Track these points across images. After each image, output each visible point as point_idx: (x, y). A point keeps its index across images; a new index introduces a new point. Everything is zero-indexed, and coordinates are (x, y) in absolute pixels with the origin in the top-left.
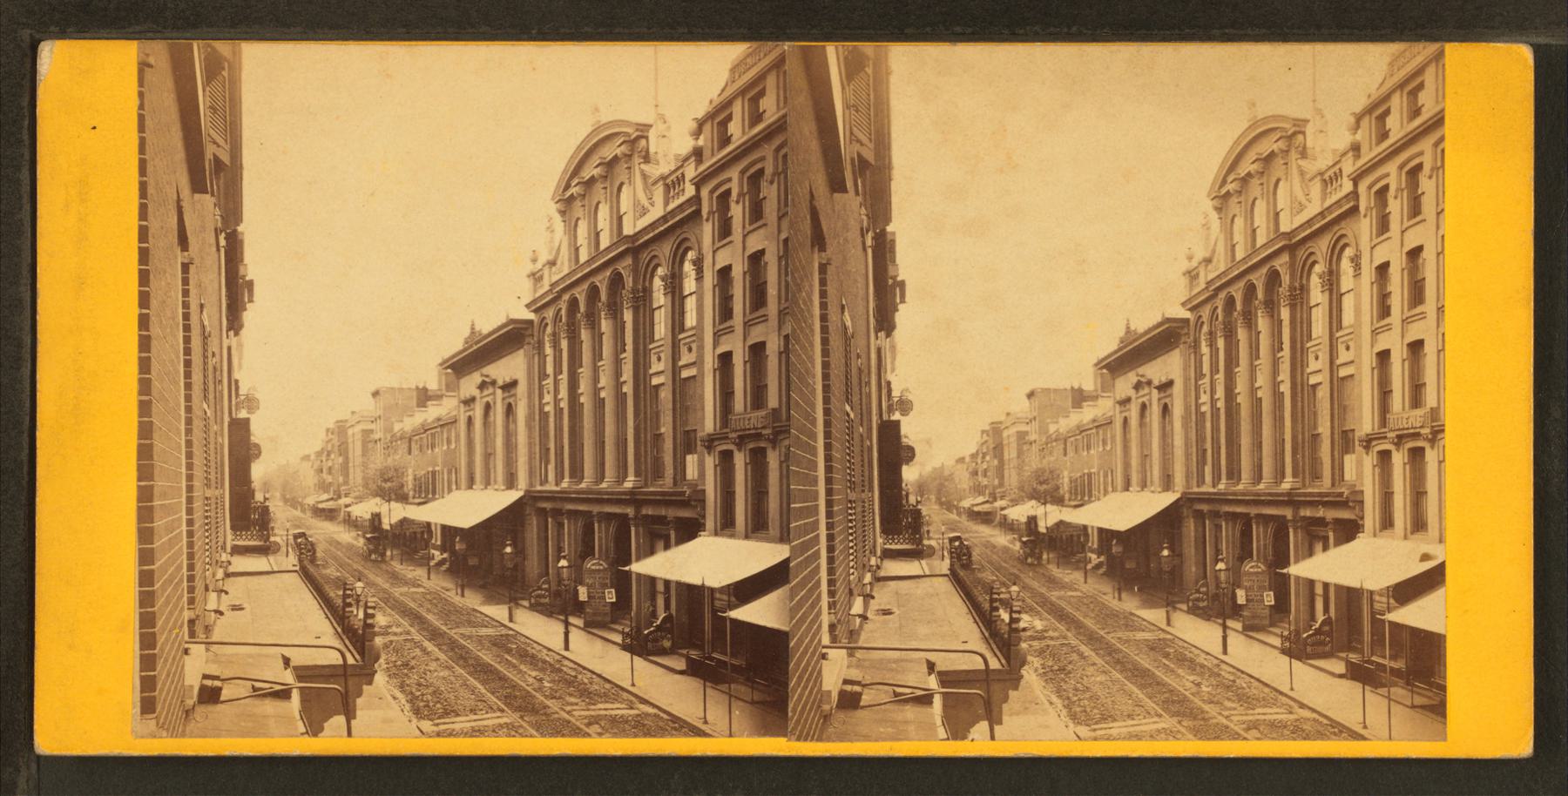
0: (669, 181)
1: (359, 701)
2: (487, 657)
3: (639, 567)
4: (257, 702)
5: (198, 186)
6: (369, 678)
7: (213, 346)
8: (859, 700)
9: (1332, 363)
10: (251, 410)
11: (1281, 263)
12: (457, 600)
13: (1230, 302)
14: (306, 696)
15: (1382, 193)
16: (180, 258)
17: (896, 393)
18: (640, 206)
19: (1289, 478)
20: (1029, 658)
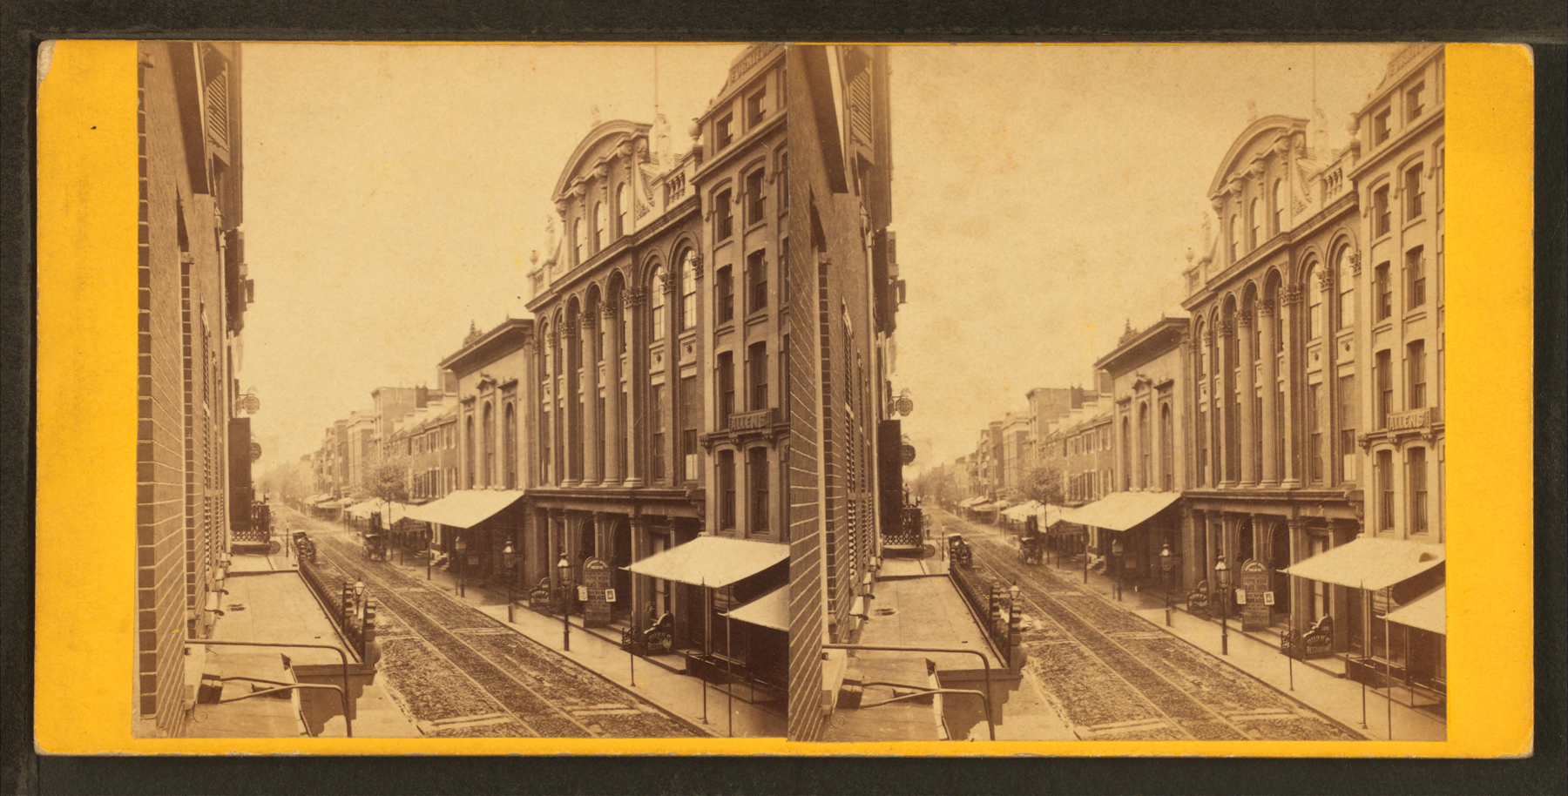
0: (669, 181)
1: (359, 701)
2: (487, 657)
3: (639, 567)
4: (257, 702)
5: (198, 186)
6: (369, 678)
7: (213, 346)
8: (859, 700)
9: (1332, 363)
10: (251, 410)
11: (624, 266)
12: (457, 599)
13: (1230, 302)
15: (1382, 193)
16: (180, 258)
17: (896, 393)
18: (640, 206)
19: (1289, 478)
20: (1029, 658)
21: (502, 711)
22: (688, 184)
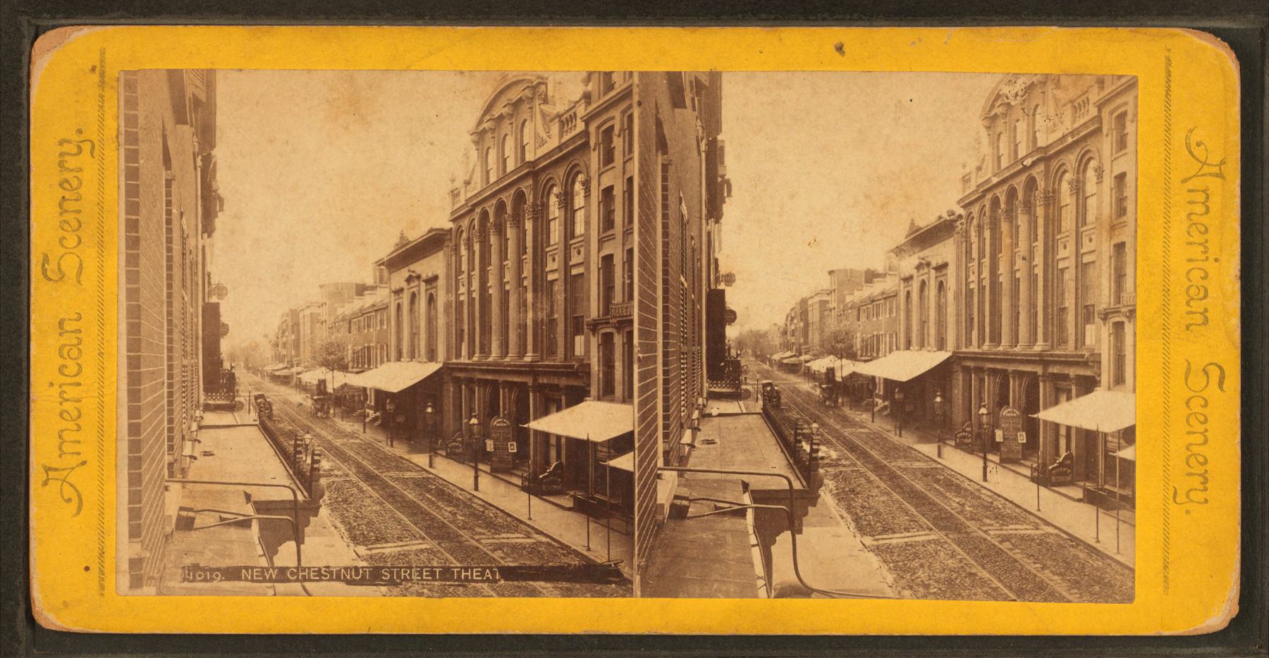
0: (563, 118)
1: (307, 530)
2: (411, 496)
3: (534, 425)
5: (180, 119)
9: (1077, 251)
10: (220, 296)
12: (387, 449)
14: (264, 526)
16: (164, 174)
18: (540, 139)
19: (1040, 342)
20: (826, 481)
21: (423, 539)
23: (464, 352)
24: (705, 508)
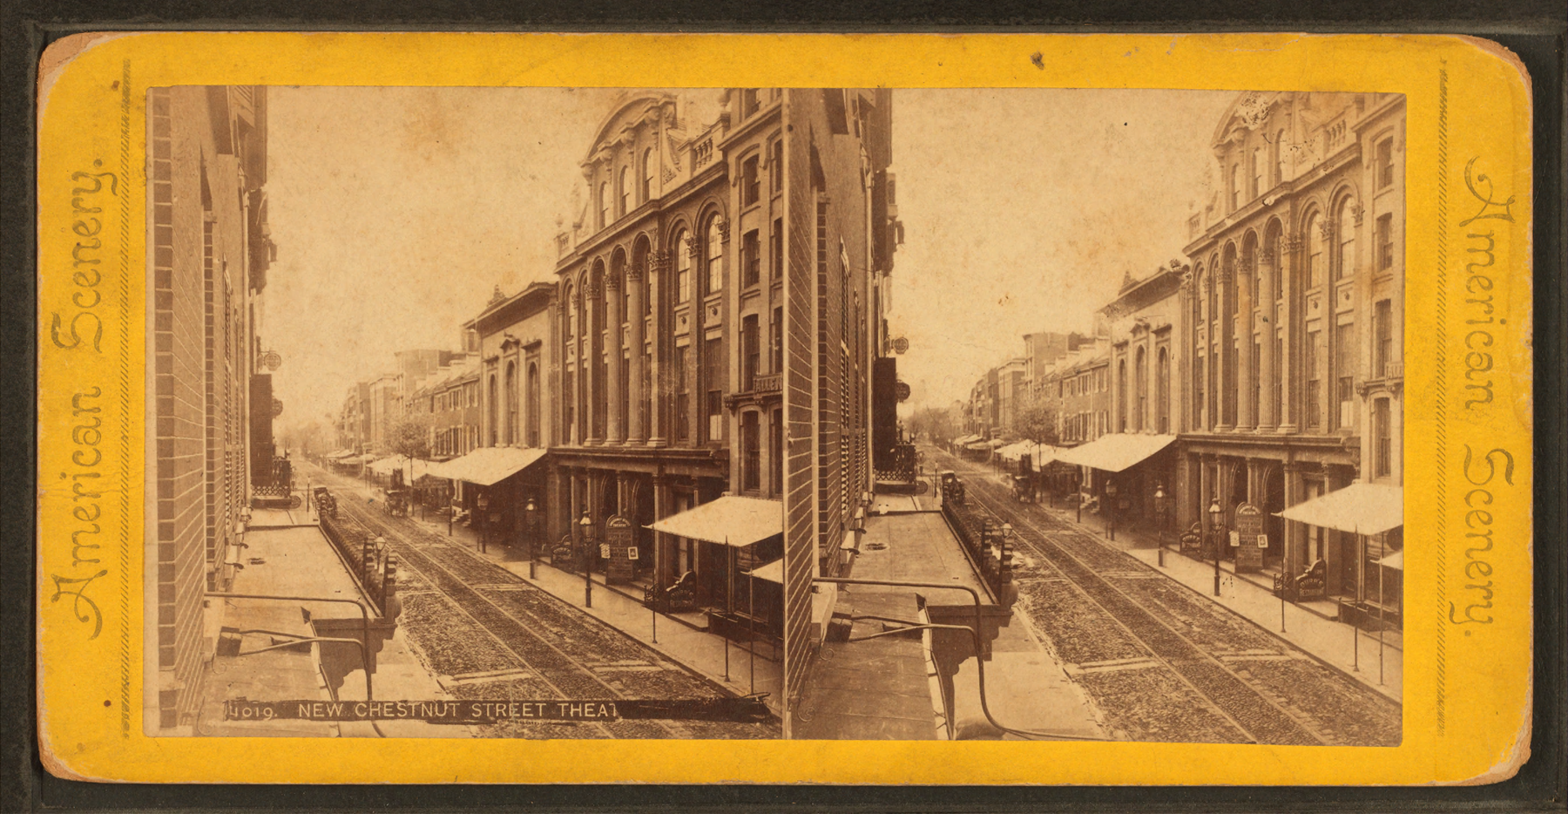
1: (379, 655)
3: (660, 526)
5: (223, 147)
9: (1331, 310)
10: (272, 366)
12: (479, 555)
14: (326, 651)
16: (203, 216)
18: (668, 172)
19: (1285, 423)
20: (1020, 595)
21: (523, 666)
22: (715, 149)
23: (1204, 423)
24: (871, 629)
